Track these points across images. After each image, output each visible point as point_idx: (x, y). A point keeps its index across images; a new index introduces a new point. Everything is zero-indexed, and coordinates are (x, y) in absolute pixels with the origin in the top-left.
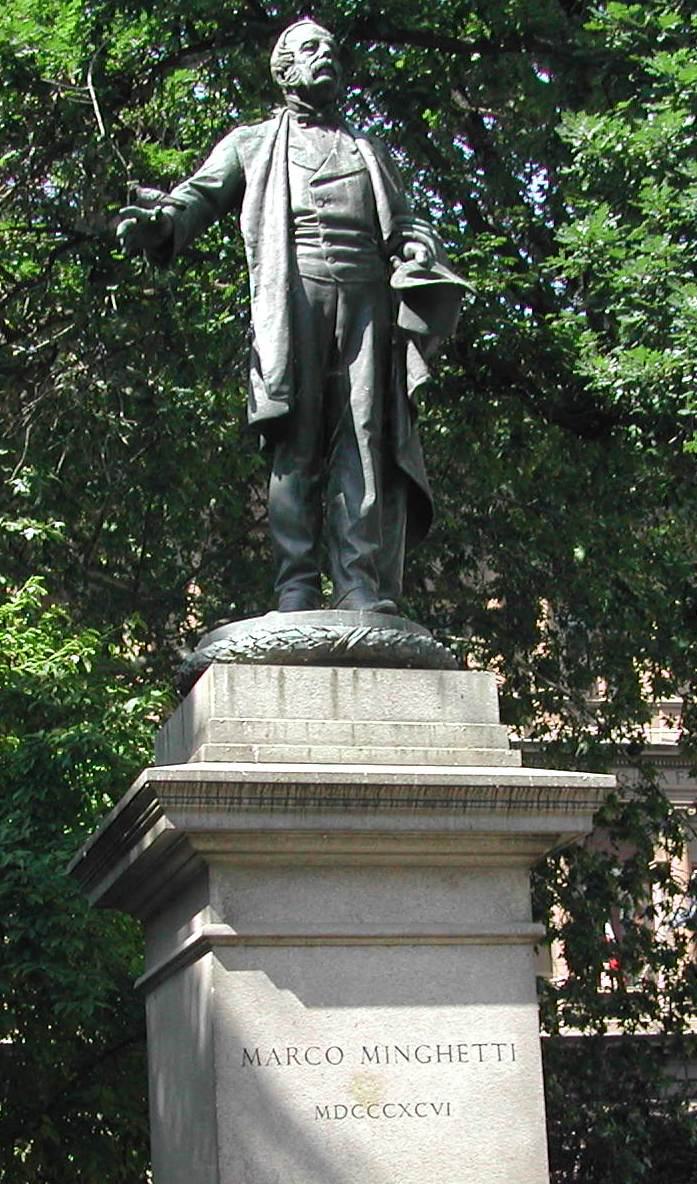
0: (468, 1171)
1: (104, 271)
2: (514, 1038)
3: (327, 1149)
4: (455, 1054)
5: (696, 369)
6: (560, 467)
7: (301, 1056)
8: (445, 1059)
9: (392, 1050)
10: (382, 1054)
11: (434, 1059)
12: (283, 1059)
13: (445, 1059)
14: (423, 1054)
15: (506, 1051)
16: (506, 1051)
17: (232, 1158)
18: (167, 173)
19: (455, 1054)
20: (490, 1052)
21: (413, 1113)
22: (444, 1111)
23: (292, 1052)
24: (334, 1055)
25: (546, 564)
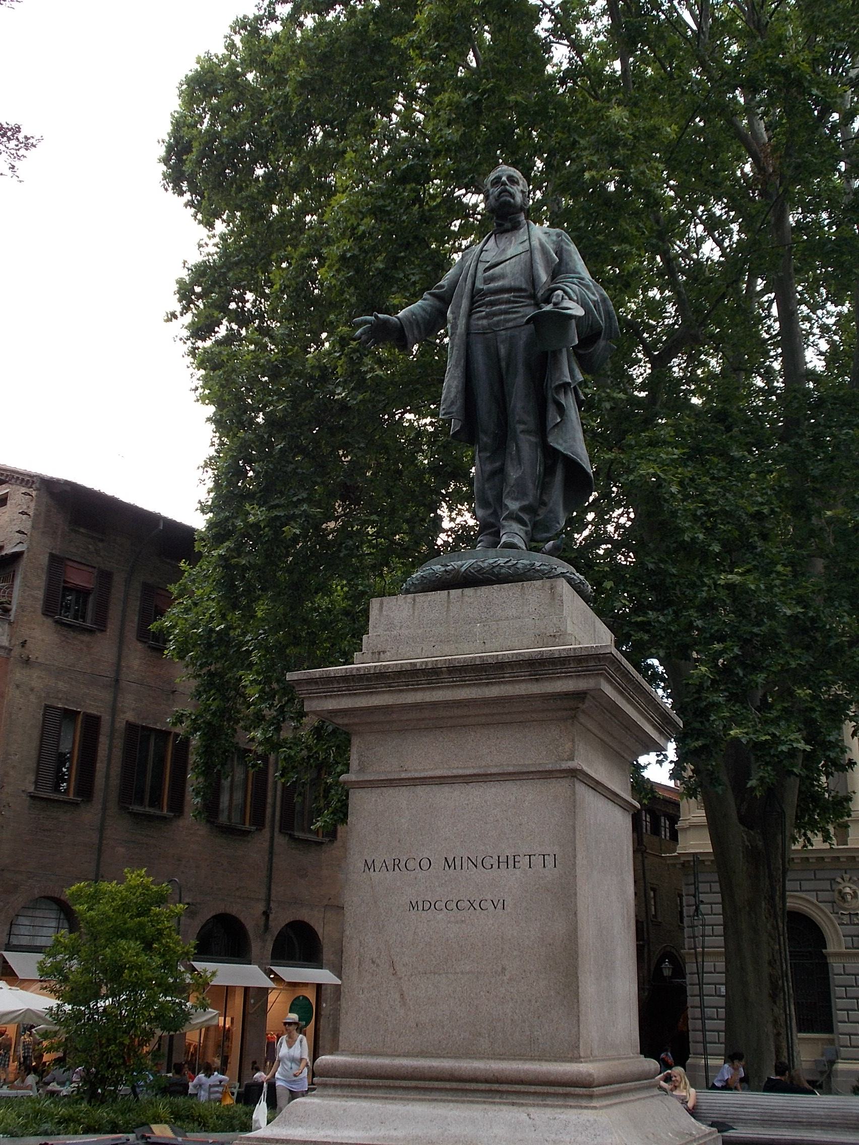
2: (556, 849)
4: (511, 862)
10: (458, 863)
11: (495, 866)
12: (390, 867)
15: (550, 860)
17: (352, 938)
19: (511, 862)
22: (500, 906)
23: (397, 862)
24: (425, 863)
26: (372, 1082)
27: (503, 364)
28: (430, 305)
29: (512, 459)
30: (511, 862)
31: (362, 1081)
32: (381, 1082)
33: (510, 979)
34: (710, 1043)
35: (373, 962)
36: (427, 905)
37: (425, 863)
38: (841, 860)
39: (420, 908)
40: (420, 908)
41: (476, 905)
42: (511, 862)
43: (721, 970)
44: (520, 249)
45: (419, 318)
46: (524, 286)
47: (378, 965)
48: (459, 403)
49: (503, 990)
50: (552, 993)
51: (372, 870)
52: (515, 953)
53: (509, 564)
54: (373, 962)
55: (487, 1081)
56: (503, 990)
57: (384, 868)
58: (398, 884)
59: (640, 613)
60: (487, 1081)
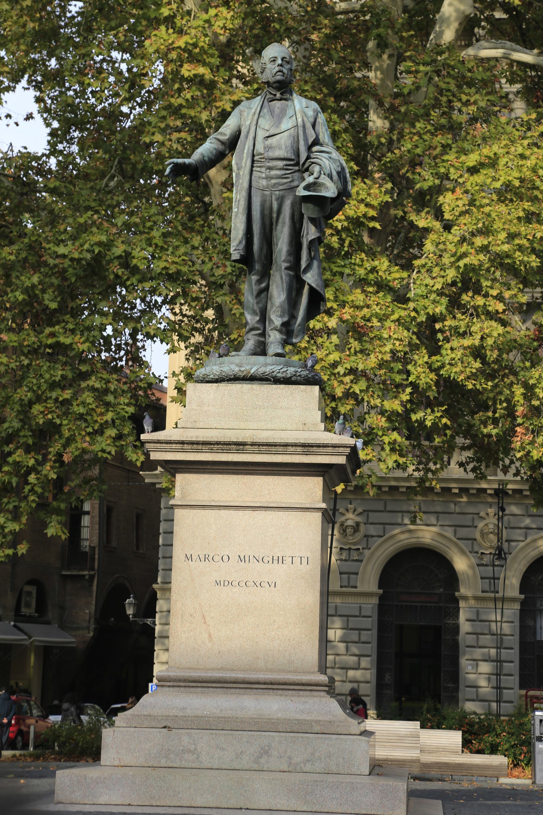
0: (281, 613)
1: (5, 721)
2: (309, 554)
3: (221, 710)
4: (280, 560)
5: (542, 328)
6: (415, 373)
7: (210, 558)
8: (275, 562)
9: (251, 557)
10: (247, 559)
11: (271, 562)
12: (203, 559)
13: (275, 562)
14: (265, 560)
15: (304, 561)
16: (304, 561)
17: (176, 601)
18: (152, 682)
19: (280, 560)
20: (297, 560)
21: (259, 585)
22: (273, 585)
23: (207, 556)
24: (226, 558)
25: (173, 55)
26: (194, 684)
27: (275, 215)
28: (215, 149)
29: (277, 286)
30: (281, 560)
31: (187, 684)
32: (199, 685)
33: (278, 627)
34: (505, 675)
35: (191, 616)
36: (226, 583)
37: (226, 558)
38: (401, 490)
39: (222, 584)
40: (222, 584)
41: (258, 584)
42: (281, 560)
43: (369, 614)
44: (290, 125)
45: (206, 159)
46: (293, 157)
47: (194, 618)
48: (244, 242)
49: (273, 633)
50: (303, 636)
51: (190, 560)
52: (281, 613)
53: (283, 370)
54: (191, 616)
55: (265, 683)
56: (273, 633)
57: (198, 560)
58: (208, 569)
59: (300, 327)
60: (265, 683)
